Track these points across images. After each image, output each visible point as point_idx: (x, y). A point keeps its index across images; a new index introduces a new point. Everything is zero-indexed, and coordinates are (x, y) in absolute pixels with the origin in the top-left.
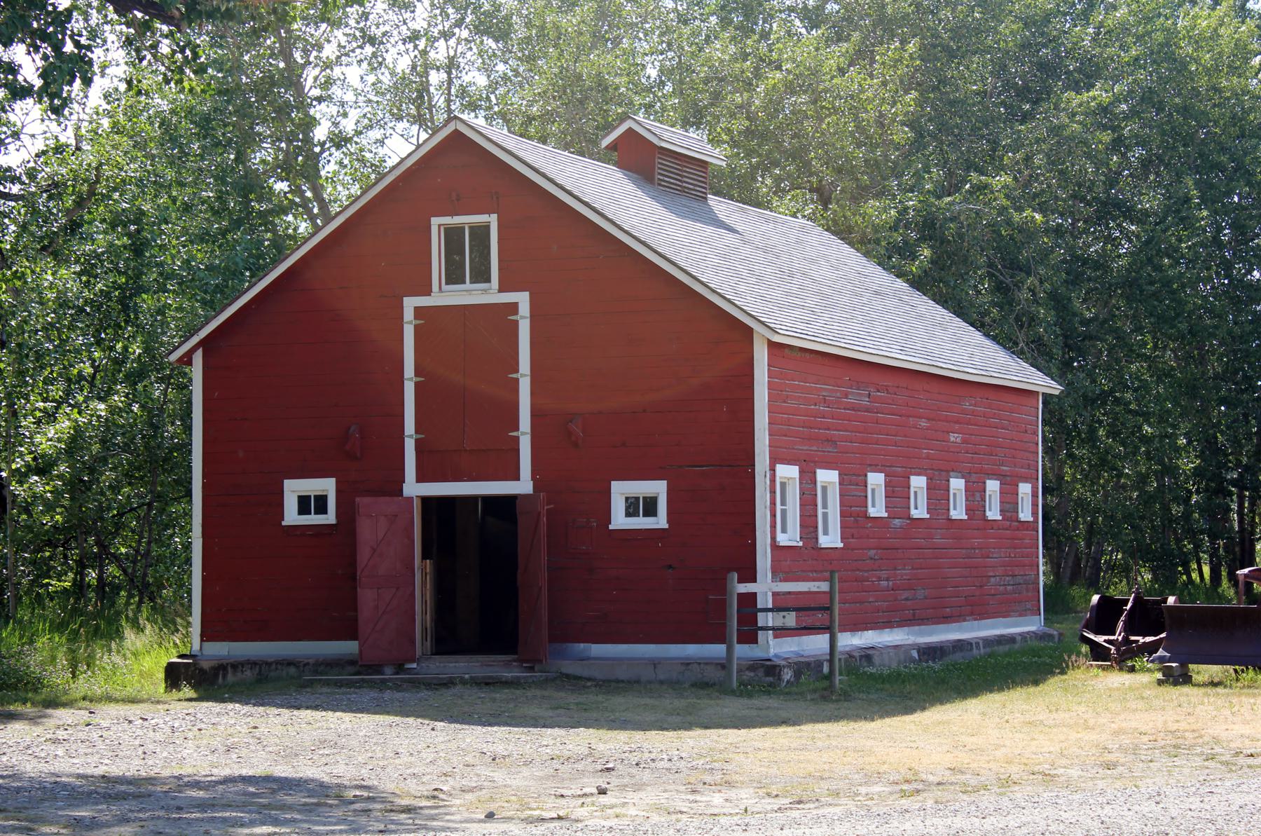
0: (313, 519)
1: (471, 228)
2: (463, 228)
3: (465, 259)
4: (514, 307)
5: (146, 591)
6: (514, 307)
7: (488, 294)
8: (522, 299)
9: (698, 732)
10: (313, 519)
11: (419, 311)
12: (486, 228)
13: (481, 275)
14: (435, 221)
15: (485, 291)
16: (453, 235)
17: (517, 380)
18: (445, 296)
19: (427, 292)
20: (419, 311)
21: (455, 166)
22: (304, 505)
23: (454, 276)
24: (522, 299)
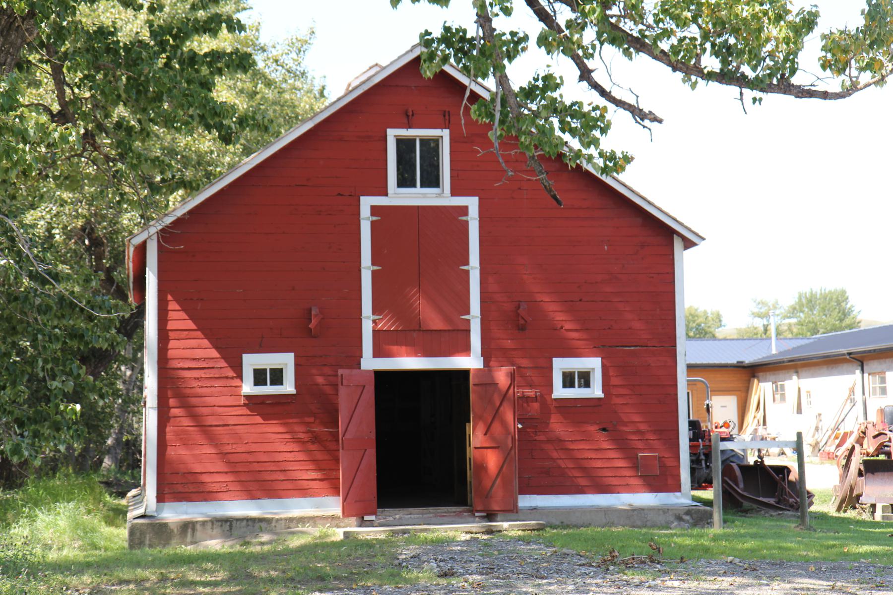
0: (269, 390)
1: (422, 141)
2: (415, 140)
3: (419, 166)
4: (464, 210)
5: (85, 464)
6: (464, 210)
7: (439, 197)
8: (472, 203)
9: (155, 494)
10: (269, 390)
11: (375, 210)
12: (437, 141)
13: (431, 180)
14: (445, 134)
15: (439, 196)
16: (405, 147)
17: (373, 264)
18: (399, 197)
19: (385, 194)
20: (375, 210)
21: (419, 87)
22: (277, 377)
23: (405, 181)
24: (472, 203)
